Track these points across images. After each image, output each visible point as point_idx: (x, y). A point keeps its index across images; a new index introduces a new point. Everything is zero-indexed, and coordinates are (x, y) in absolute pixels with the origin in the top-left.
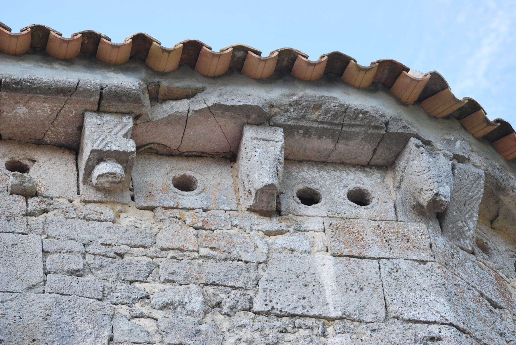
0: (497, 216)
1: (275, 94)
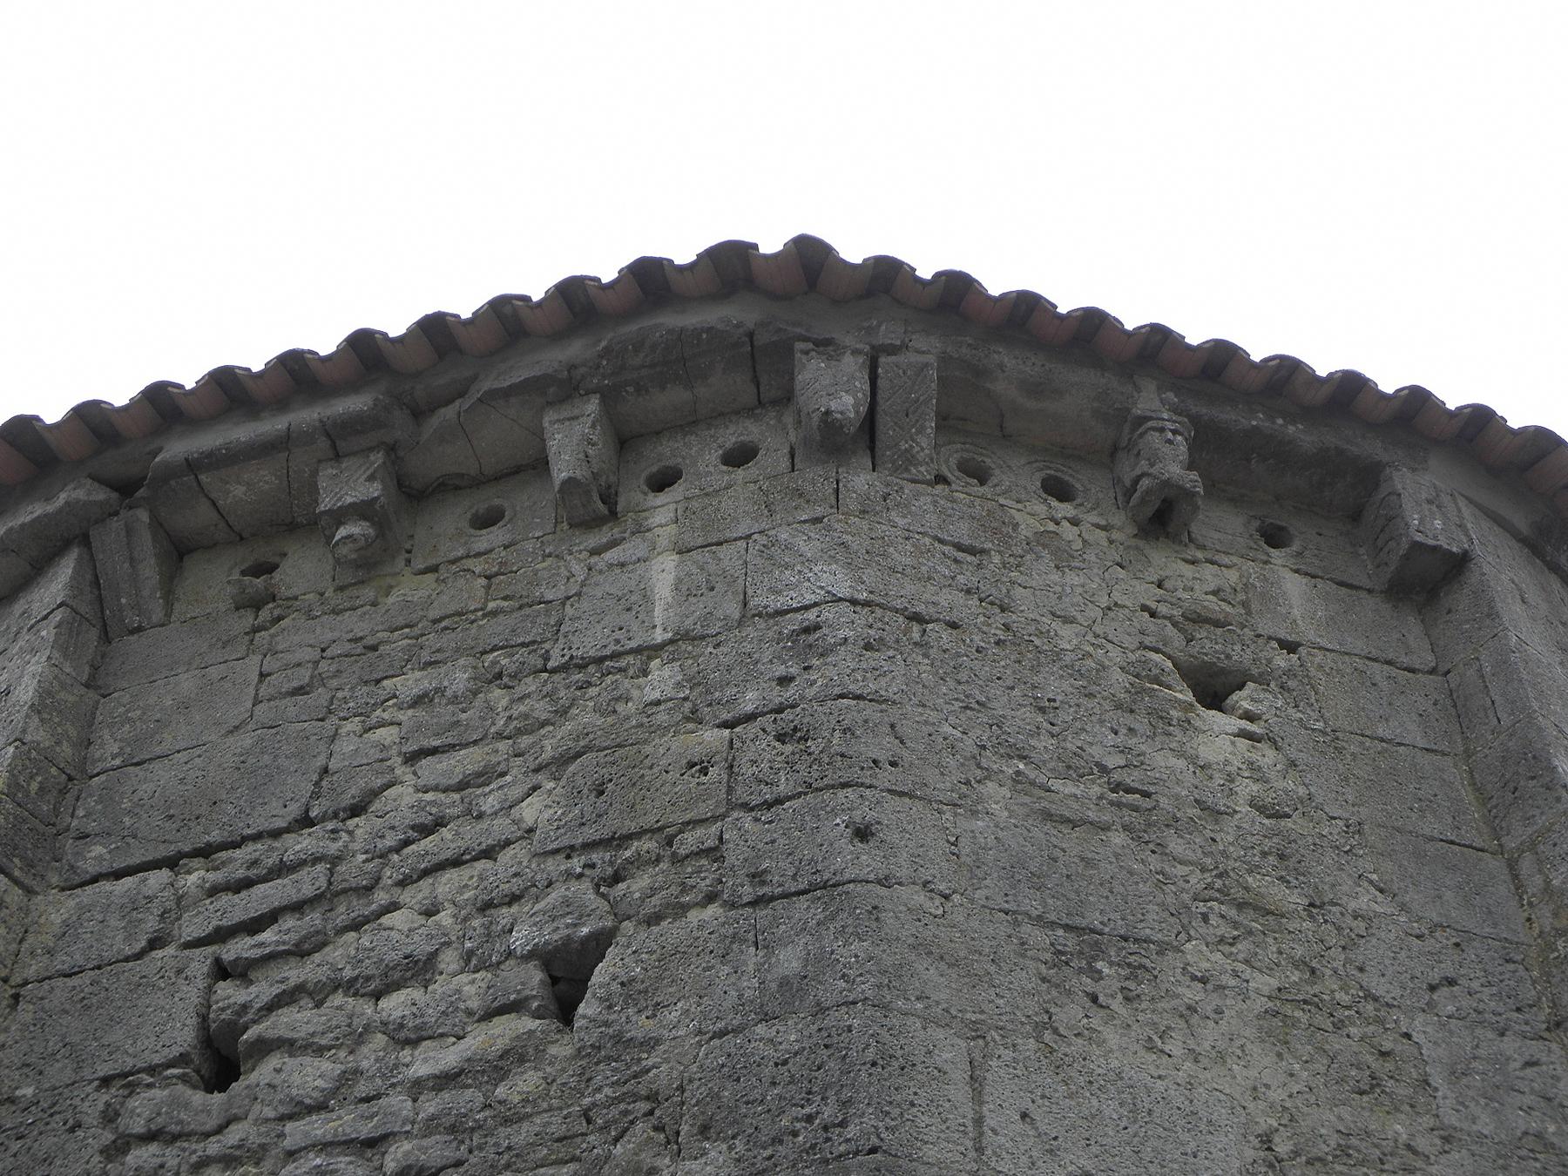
0: (1002, 416)
1: (576, 350)
